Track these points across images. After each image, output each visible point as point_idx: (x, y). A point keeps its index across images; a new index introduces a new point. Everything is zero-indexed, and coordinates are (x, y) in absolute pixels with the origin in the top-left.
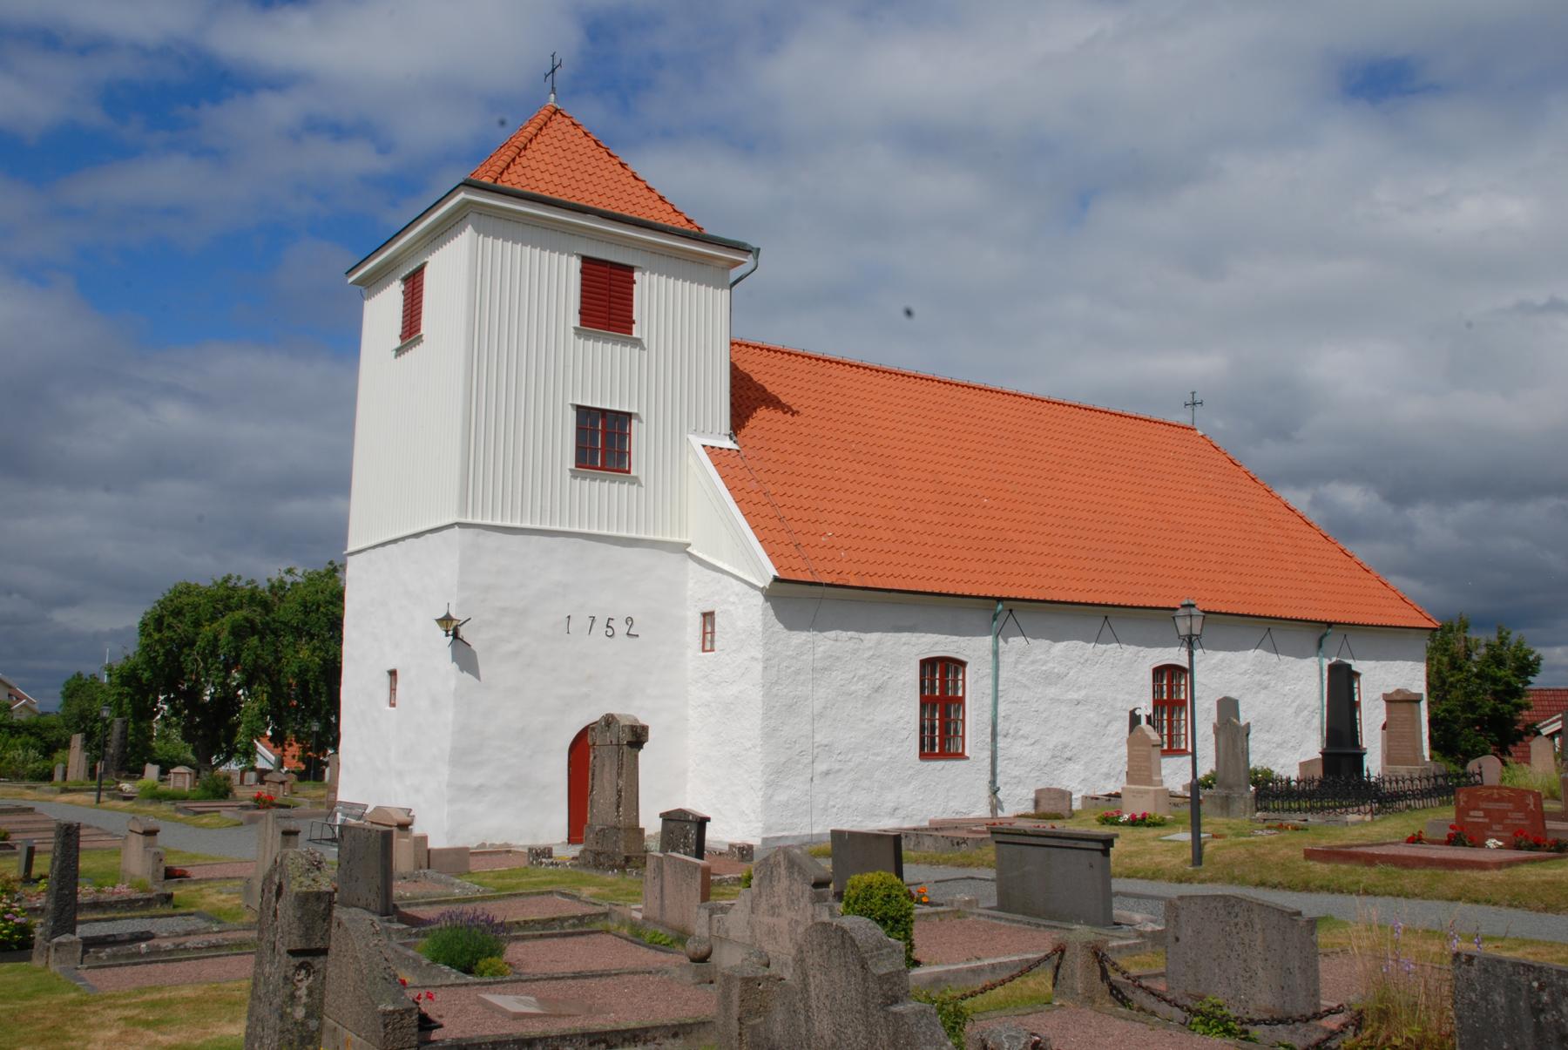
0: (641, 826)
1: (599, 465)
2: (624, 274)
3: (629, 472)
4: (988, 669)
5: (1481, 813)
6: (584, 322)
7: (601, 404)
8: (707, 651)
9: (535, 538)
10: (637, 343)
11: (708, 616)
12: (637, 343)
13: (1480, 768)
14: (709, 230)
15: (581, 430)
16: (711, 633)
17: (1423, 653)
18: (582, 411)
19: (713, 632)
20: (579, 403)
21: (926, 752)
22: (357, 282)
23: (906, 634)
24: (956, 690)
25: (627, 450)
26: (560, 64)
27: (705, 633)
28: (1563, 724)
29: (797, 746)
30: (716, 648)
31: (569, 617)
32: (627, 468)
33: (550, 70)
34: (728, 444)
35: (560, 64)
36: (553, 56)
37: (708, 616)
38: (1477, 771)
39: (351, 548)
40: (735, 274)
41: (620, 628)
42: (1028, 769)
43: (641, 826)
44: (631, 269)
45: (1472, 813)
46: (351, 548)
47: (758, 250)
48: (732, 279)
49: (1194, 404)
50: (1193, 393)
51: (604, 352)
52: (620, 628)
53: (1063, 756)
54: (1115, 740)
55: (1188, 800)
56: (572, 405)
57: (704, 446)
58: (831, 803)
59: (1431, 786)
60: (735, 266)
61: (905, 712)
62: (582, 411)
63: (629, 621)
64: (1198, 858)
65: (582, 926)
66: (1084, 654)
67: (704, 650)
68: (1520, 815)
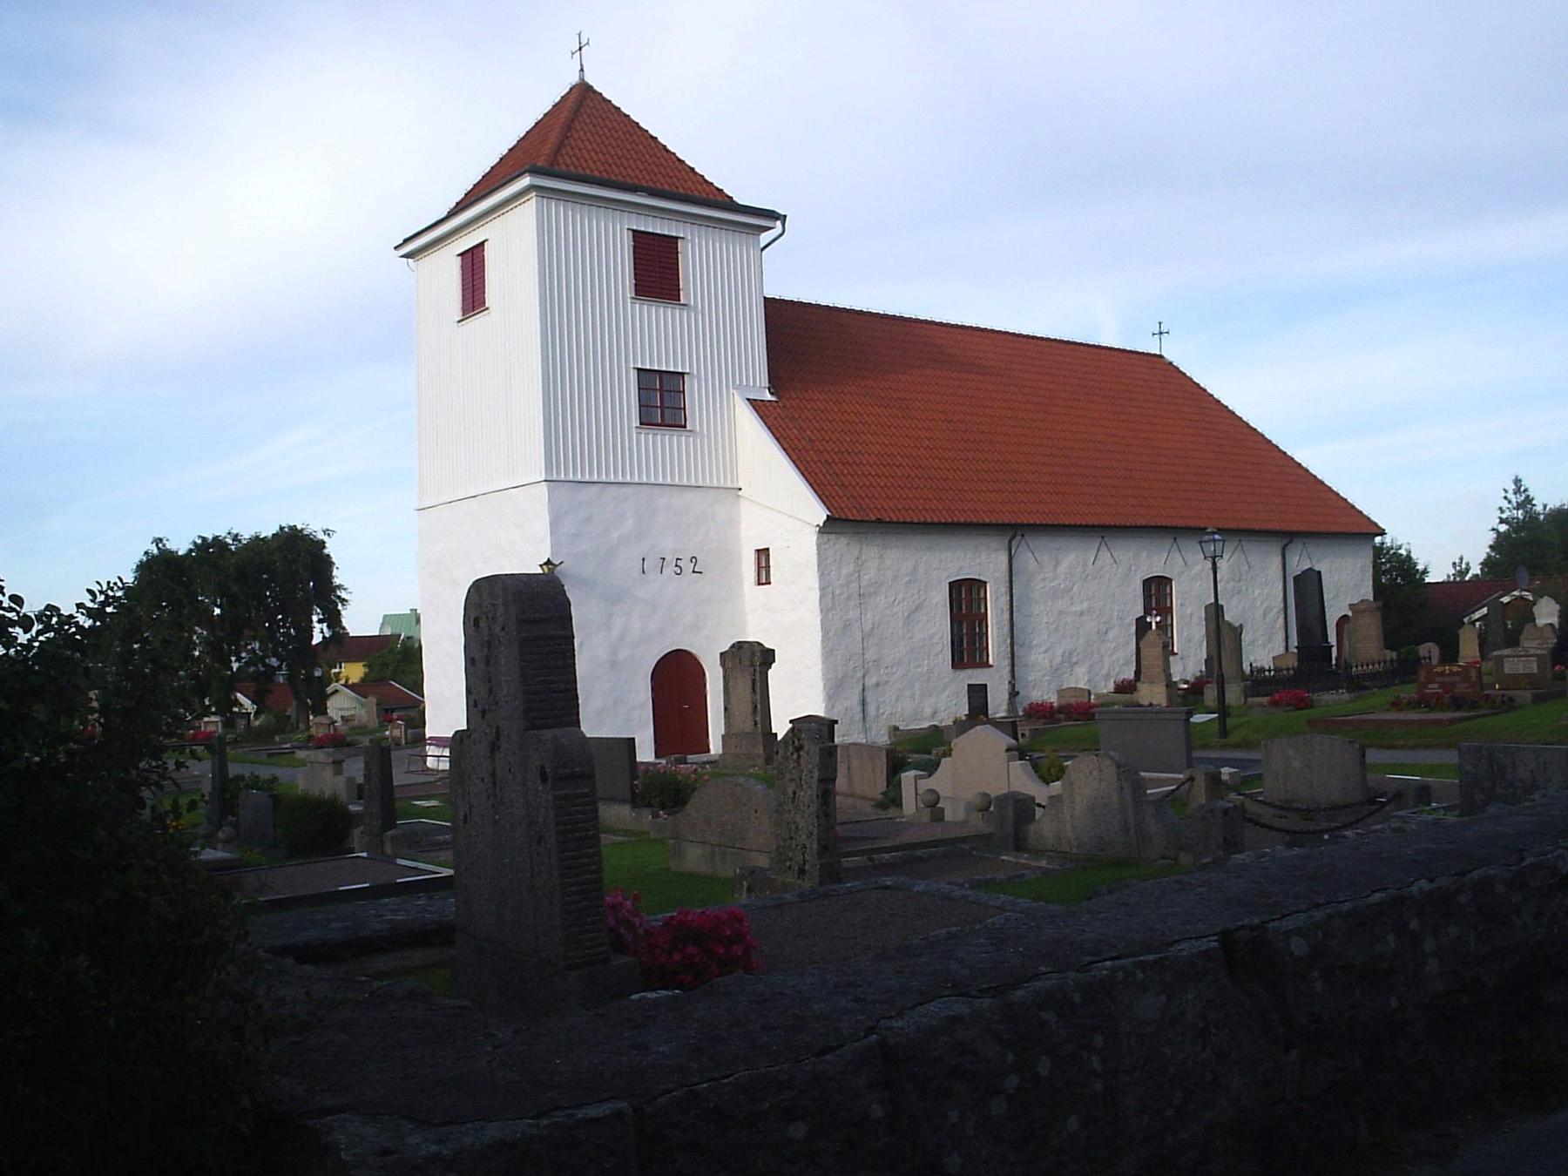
0: (774, 731)
2: (669, 246)
3: (685, 427)
4: (1004, 589)
5: (1436, 686)
6: (638, 292)
7: (650, 365)
8: (763, 584)
11: (763, 554)
13: (1430, 652)
14: (1019, 549)
16: (766, 567)
19: (768, 567)
20: (640, 366)
24: (979, 608)
26: (573, 54)
27: (759, 567)
28: (1488, 610)
29: (852, 662)
30: (772, 581)
32: (683, 423)
33: (583, 49)
34: (768, 397)
35: (573, 54)
36: (579, 35)
37: (763, 554)
38: (1427, 655)
40: (765, 238)
41: (687, 566)
42: (1042, 674)
43: (774, 731)
45: (1430, 686)
47: (785, 216)
48: (762, 245)
49: (1161, 333)
50: (1160, 323)
51: (656, 314)
52: (687, 566)
53: (1069, 662)
54: (1114, 645)
55: (448, 759)
56: (634, 368)
57: (748, 400)
58: (881, 711)
59: (1381, 669)
60: (766, 231)
61: (938, 626)
64: (1224, 732)
65: (1223, 747)
66: (1085, 571)
67: (759, 584)
68: (1467, 685)
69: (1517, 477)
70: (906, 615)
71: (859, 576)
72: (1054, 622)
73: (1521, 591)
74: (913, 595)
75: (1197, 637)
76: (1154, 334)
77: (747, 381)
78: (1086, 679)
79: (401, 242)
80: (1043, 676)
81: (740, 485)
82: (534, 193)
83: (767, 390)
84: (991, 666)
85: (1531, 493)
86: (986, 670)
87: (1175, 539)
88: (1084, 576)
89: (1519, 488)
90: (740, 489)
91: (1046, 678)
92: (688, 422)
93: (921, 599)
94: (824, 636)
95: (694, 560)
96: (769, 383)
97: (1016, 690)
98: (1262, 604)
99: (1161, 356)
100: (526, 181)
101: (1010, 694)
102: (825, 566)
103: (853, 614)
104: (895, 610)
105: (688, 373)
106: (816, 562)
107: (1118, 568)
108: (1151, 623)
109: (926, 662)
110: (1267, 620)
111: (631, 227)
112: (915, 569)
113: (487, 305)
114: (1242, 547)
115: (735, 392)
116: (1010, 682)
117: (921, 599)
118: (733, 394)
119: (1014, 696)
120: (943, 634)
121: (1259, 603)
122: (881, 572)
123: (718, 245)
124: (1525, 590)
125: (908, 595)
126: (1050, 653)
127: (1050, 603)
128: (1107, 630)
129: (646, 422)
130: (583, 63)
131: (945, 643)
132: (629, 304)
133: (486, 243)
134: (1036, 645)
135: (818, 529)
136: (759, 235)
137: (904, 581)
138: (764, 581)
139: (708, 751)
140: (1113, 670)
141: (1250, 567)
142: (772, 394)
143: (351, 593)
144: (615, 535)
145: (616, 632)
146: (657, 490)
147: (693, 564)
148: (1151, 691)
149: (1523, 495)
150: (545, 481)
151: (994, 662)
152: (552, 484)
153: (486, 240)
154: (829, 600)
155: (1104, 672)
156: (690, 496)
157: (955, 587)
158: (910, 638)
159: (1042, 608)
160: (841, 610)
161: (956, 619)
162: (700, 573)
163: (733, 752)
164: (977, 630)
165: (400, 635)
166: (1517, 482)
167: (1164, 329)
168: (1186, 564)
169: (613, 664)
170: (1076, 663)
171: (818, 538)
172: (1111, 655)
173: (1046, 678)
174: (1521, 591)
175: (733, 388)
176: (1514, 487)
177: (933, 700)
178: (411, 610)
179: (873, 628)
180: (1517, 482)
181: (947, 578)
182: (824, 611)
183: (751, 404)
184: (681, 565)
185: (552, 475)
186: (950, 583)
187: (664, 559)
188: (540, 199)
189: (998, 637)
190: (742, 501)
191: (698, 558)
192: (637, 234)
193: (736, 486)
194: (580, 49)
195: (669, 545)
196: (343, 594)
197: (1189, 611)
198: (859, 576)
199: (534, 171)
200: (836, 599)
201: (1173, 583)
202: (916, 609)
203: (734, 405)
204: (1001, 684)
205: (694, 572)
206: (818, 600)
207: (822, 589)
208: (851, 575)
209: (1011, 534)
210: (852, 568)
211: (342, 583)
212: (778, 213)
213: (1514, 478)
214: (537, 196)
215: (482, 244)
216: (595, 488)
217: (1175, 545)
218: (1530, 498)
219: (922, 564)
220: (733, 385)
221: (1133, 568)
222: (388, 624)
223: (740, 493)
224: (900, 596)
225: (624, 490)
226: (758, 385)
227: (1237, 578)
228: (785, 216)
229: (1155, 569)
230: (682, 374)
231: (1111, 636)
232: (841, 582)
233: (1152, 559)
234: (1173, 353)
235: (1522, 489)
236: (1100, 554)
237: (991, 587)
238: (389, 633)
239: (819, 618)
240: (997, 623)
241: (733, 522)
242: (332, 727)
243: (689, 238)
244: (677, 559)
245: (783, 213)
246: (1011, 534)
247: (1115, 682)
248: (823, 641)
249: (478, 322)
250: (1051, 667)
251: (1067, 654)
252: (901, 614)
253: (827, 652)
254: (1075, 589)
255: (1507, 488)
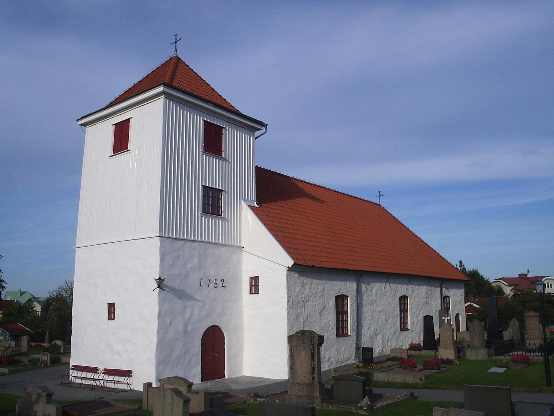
1: (211, 212)
4: (355, 300)
9: (549, 280)
10: (224, 159)
12: (224, 159)
15: (204, 196)
17: (463, 286)
18: (204, 187)
20: (204, 184)
21: (338, 335)
22: (81, 125)
23: (356, 287)
25: (221, 206)
26: (180, 39)
31: (201, 279)
32: (221, 214)
35: (180, 39)
37: (254, 281)
39: (77, 246)
40: (257, 133)
42: (367, 339)
44: (222, 128)
46: (77, 246)
47: (267, 125)
49: (380, 196)
50: (379, 192)
51: (212, 161)
62: (204, 187)
63: (223, 280)
67: (251, 293)
69: (460, 260)
70: (320, 311)
71: (303, 292)
72: (371, 315)
73: (470, 303)
74: (322, 302)
75: (416, 322)
76: (376, 196)
77: (247, 198)
78: (382, 341)
79: (81, 118)
80: (367, 340)
81: (243, 245)
82: (163, 96)
83: (255, 202)
84: (350, 336)
85: (465, 267)
86: (348, 337)
87: (409, 280)
88: (381, 295)
89: (461, 265)
90: (243, 247)
91: (368, 341)
92: (223, 214)
93: (325, 304)
94: (288, 321)
95: (222, 280)
96: (256, 199)
97: (359, 347)
98: (435, 308)
99: (380, 205)
100: (161, 89)
101: (356, 349)
102: (290, 286)
103: (299, 311)
104: (316, 309)
105: (224, 190)
106: (286, 285)
107: (392, 291)
108: (445, 319)
109: (327, 334)
110: (436, 315)
111: (204, 119)
112: (323, 289)
113: (129, 149)
114: (388, 280)
115: (242, 201)
116: (356, 343)
117: (325, 304)
118: (242, 202)
119: (358, 350)
120: (333, 321)
121: (434, 308)
122: (311, 290)
123: (241, 133)
124: (472, 302)
125: (321, 302)
126: (369, 330)
127: (369, 307)
128: (388, 319)
129: (205, 211)
130: (177, 48)
131: (334, 325)
132: (201, 155)
133: (131, 119)
134: (365, 326)
135: (287, 268)
136: (255, 132)
137: (319, 295)
138: (253, 292)
139: (224, 377)
140: (390, 337)
141: (431, 293)
142: (257, 204)
143: (7, 284)
144: (189, 266)
145: (187, 315)
146: (208, 245)
147: (222, 283)
148: (446, 352)
149: (462, 267)
150: (159, 236)
151: (351, 334)
152: (162, 238)
153: (131, 118)
154: (291, 303)
155: (387, 338)
156: (222, 249)
157: (337, 297)
158: (321, 322)
159: (367, 309)
160: (295, 308)
161: (338, 313)
162: (225, 287)
163: (296, 394)
164: (344, 318)
165: (15, 301)
166: (461, 262)
167: (381, 194)
168: (413, 291)
169: (185, 332)
170: (378, 334)
171: (287, 273)
172: (389, 331)
173: (368, 341)
174: (470, 303)
175: (242, 200)
176: (459, 264)
177: (329, 352)
178: (18, 290)
179: (307, 317)
180: (461, 262)
181: (335, 294)
182: (289, 309)
183: (250, 207)
184: (217, 283)
185: (162, 234)
186: (336, 297)
187: (210, 279)
188: (166, 99)
189: (352, 322)
190: (243, 253)
191: (224, 280)
192: (206, 123)
193: (241, 245)
194: (176, 42)
195: (212, 273)
196: (3, 284)
197: (413, 311)
198: (303, 292)
199: (165, 85)
200: (294, 303)
201: (408, 298)
202: (323, 308)
203: (242, 208)
204: (353, 344)
205: (222, 286)
206: (286, 304)
207: (288, 298)
208: (299, 291)
209: (21, 292)
210: (300, 288)
211: (3, 279)
212: (264, 123)
213: (459, 261)
214: (164, 97)
215: (129, 120)
216: (182, 242)
217: (387, 281)
218: (465, 268)
219: (326, 287)
220: (242, 199)
221: (396, 292)
222: (10, 296)
223: (243, 249)
224: (318, 302)
225: (194, 244)
226: (252, 199)
227: (428, 297)
228: (267, 125)
229: (403, 293)
230: (222, 191)
231: (389, 321)
232: (296, 295)
233: (403, 289)
234: (384, 203)
235: (462, 265)
236: (386, 285)
237: (350, 299)
238: (9, 299)
239: (287, 312)
240: (352, 316)
241: (239, 263)
242: (5, 351)
243: (227, 128)
244: (216, 280)
245: (266, 124)
246: (21, 292)
247: (409, 345)
248: (288, 324)
249: (122, 157)
250: (370, 336)
251: (375, 329)
252: (318, 311)
253: (289, 329)
254: (378, 301)
255: (457, 264)
